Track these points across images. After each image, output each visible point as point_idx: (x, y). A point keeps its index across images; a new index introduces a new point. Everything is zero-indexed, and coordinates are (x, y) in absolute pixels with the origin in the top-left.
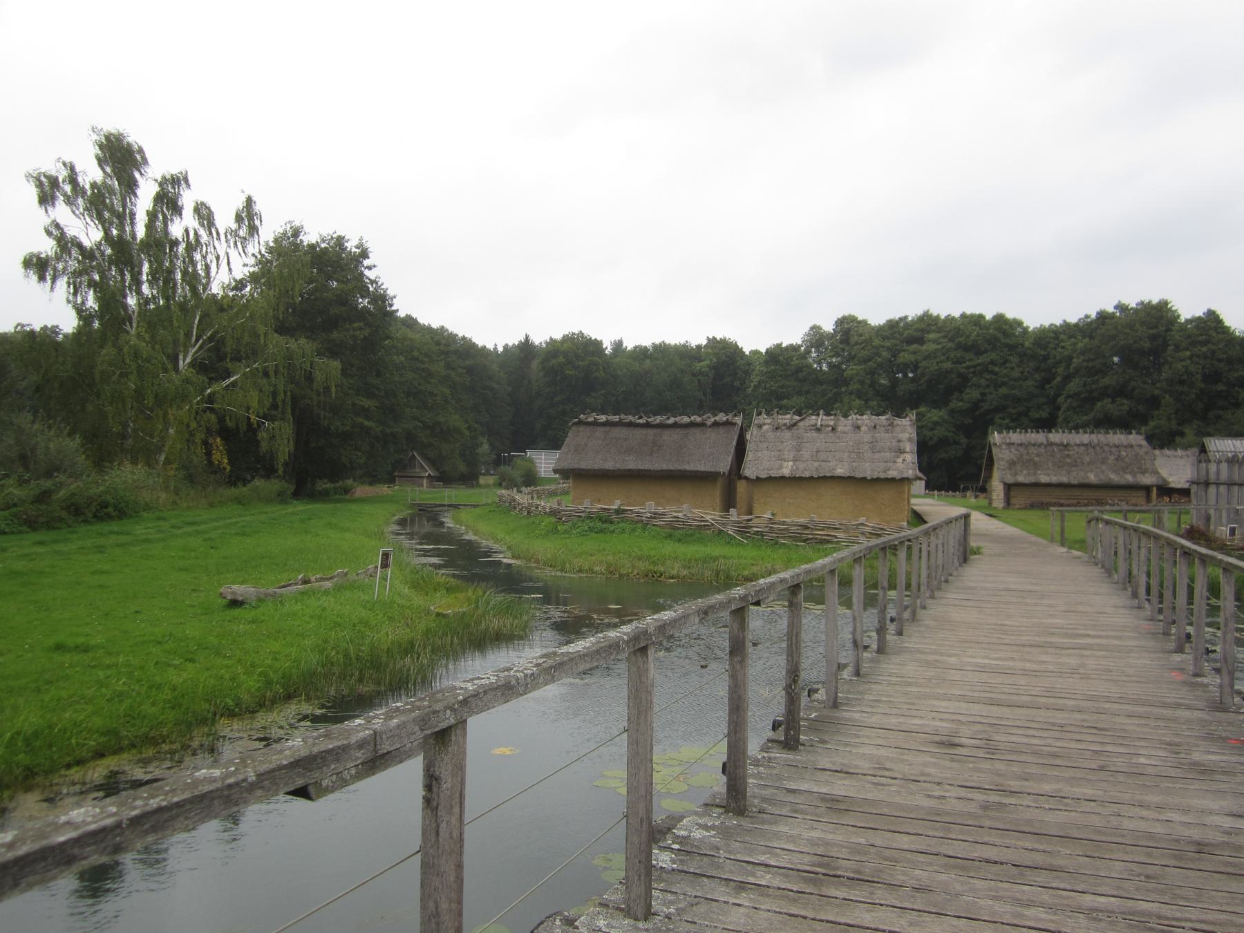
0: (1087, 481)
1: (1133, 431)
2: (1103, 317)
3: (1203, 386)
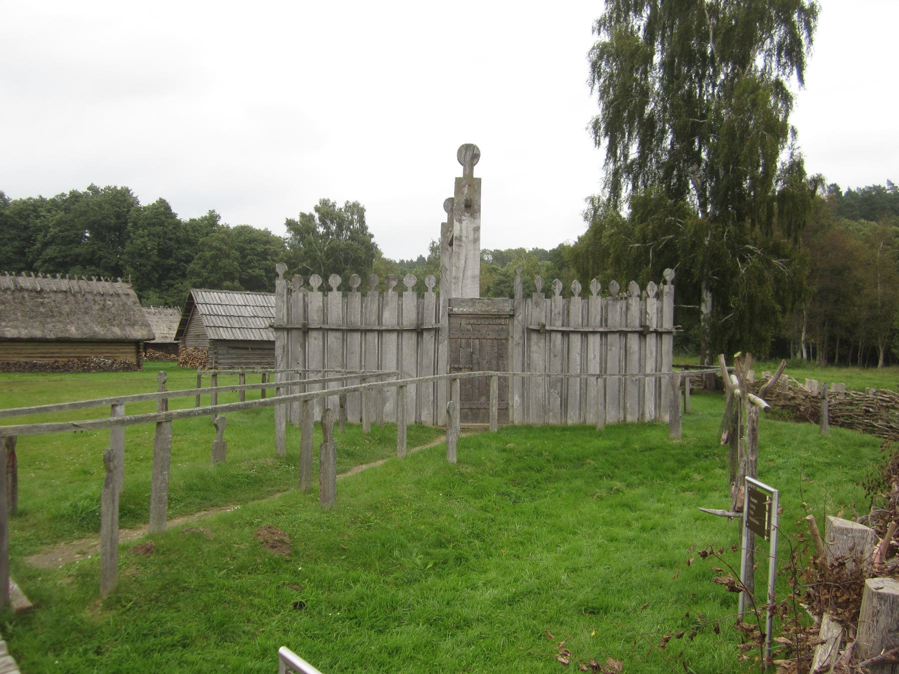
0: (67, 335)
1: (119, 279)
2: (75, 196)
3: (157, 259)
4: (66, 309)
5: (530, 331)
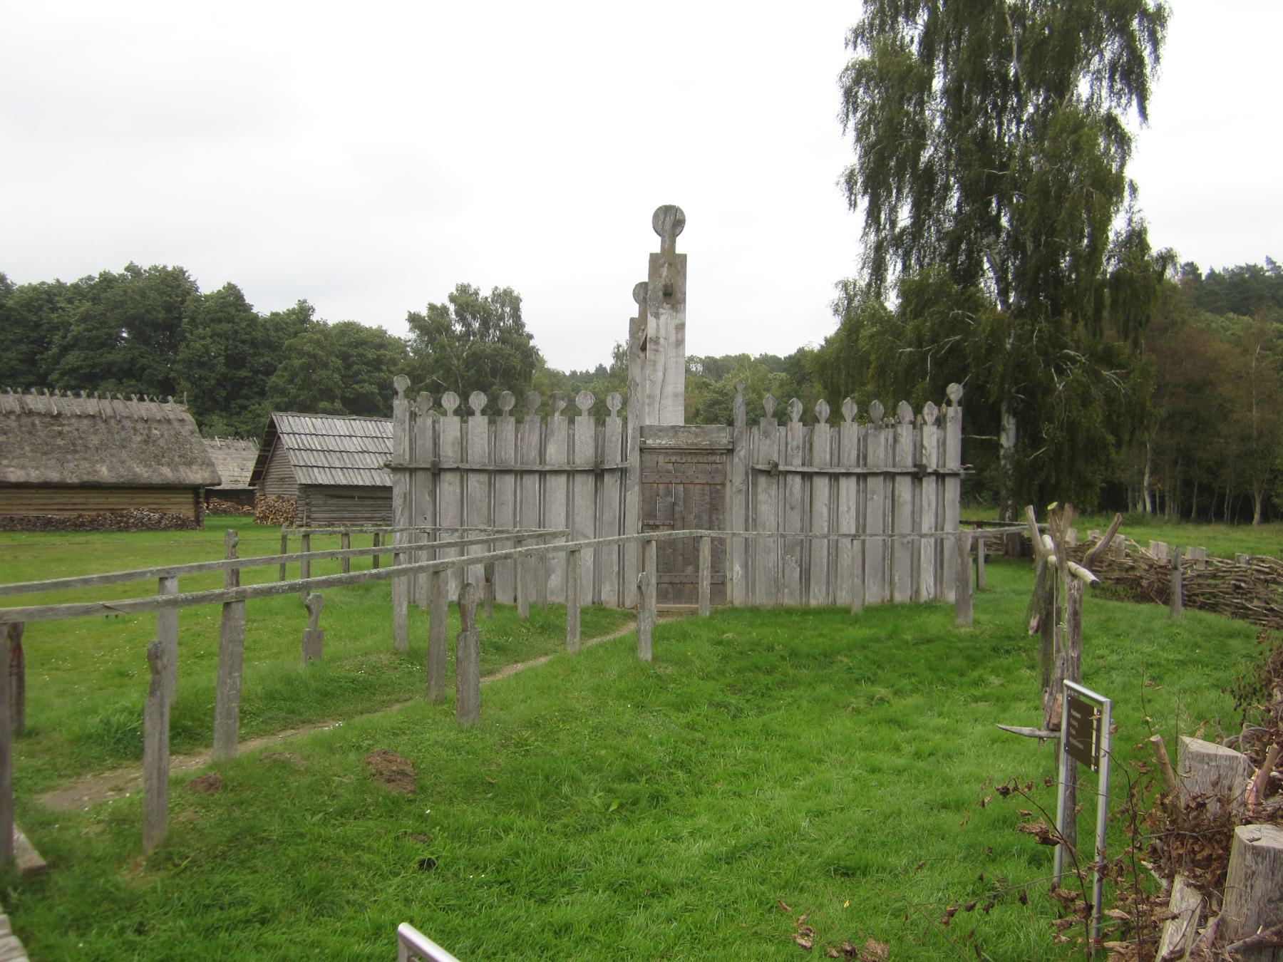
0: (96, 478)
1: (170, 398)
2: (107, 280)
3: (224, 370)
4: (94, 441)
5: (757, 472)
